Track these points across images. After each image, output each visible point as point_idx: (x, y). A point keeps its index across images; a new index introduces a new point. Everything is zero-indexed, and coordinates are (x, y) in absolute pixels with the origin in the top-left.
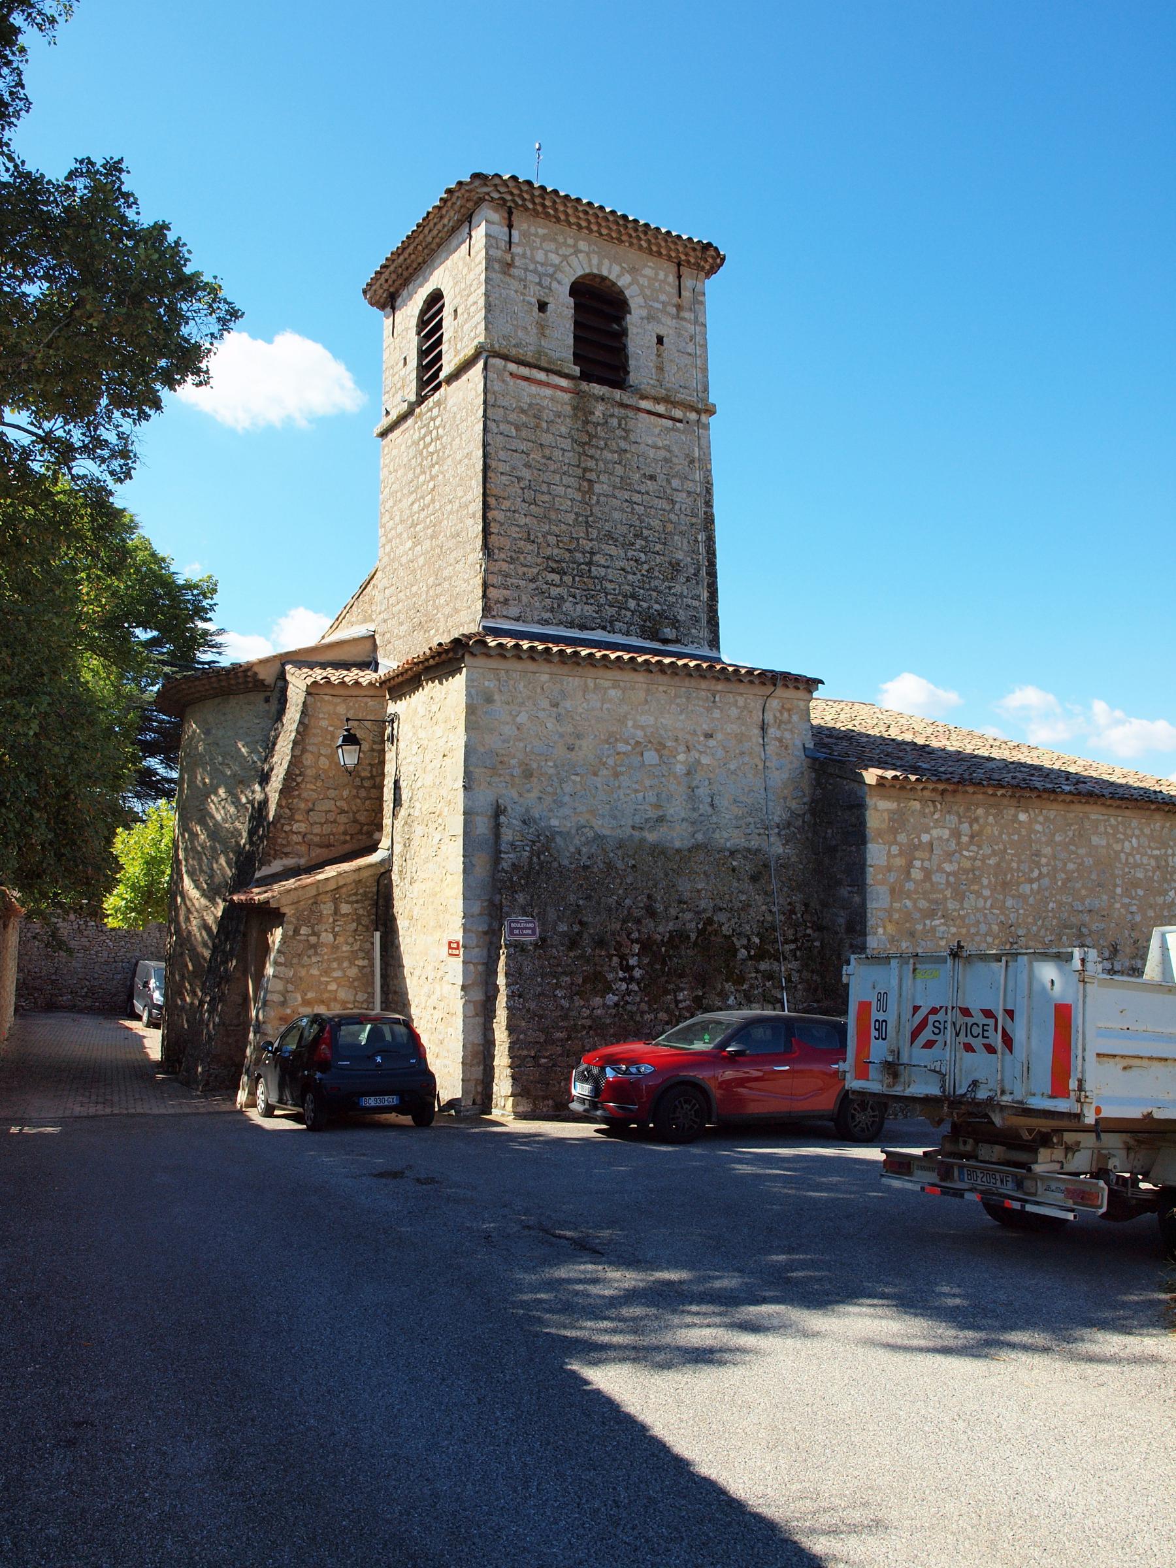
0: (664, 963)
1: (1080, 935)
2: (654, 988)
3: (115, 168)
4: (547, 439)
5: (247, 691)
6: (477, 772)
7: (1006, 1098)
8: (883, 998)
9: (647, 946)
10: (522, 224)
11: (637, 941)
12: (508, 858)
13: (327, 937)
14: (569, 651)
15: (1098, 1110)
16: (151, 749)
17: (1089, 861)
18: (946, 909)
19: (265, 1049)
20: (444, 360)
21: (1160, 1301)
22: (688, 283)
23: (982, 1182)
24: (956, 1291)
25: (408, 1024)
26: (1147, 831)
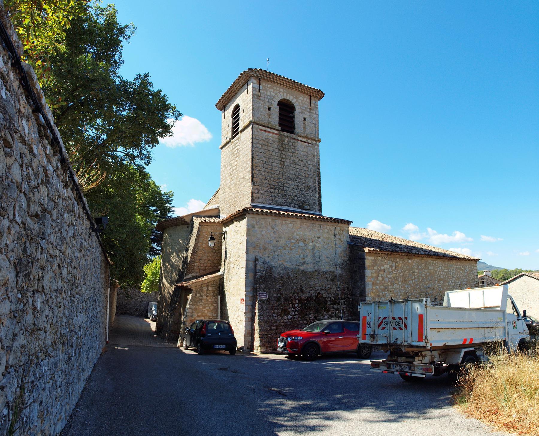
0: (305, 306)
1: (426, 295)
2: (303, 314)
3: (147, 76)
4: (271, 149)
5: (182, 224)
6: (250, 248)
7: (406, 343)
8: (370, 315)
9: (300, 301)
10: (263, 84)
11: (297, 299)
12: (259, 274)
13: (204, 297)
14: (277, 212)
15: (431, 344)
16: (154, 241)
17: (428, 274)
18: (388, 288)
19: (186, 329)
20: (240, 125)
21: (449, 398)
22: (313, 102)
23: (399, 368)
24: (393, 402)
25: (228, 324)
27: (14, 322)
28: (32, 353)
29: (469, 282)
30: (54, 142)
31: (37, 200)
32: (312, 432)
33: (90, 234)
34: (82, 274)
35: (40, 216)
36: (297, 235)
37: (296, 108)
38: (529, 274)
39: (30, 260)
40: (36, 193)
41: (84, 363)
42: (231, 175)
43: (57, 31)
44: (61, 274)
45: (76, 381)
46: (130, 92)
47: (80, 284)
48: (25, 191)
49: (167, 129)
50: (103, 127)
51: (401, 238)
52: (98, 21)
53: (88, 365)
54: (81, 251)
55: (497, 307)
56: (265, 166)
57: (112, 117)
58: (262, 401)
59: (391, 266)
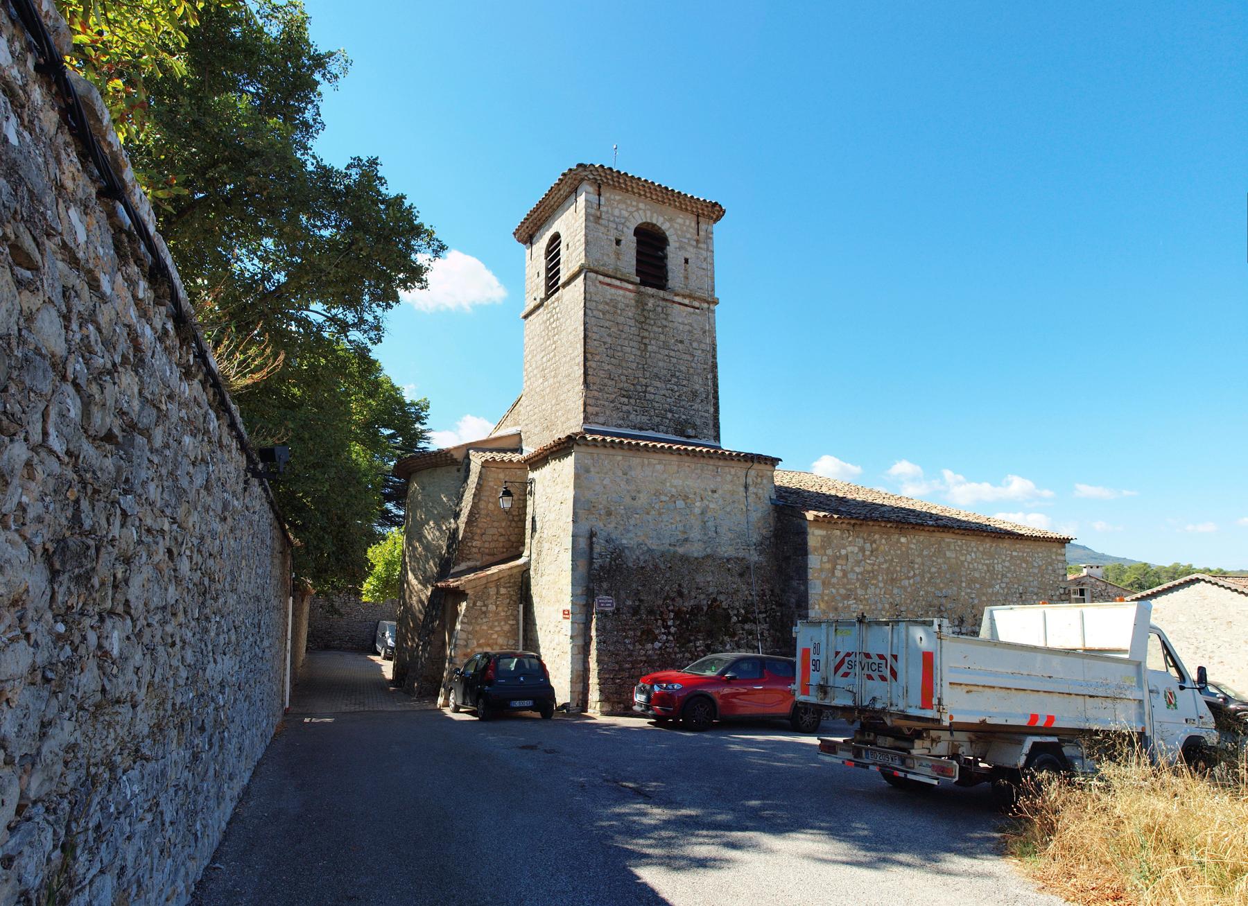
0: (688, 624)
1: (940, 611)
2: (683, 639)
3: (373, 162)
4: (621, 319)
5: (447, 465)
6: (581, 512)
8: (817, 647)
9: (678, 614)
10: (606, 194)
12: (598, 562)
13: (492, 608)
15: (951, 717)
16: (388, 498)
17: (944, 567)
20: (561, 274)
22: (703, 226)
23: (880, 759)
25: (539, 658)
27: (45, 694)
28: (98, 760)
29: (1045, 590)
30: (157, 274)
31: (110, 402)
32: (701, 871)
33: (246, 482)
34: (227, 570)
35: (120, 439)
36: (672, 486)
38: (1218, 578)
39: (91, 543)
40: (109, 387)
41: (232, 761)
42: (543, 370)
43: (166, 26)
44: (175, 570)
45: (212, 803)
46: (338, 192)
47: (223, 590)
48: (75, 378)
49: (415, 275)
50: (278, 257)
51: (883, 490)
52: (266, 30)
53: (242, 765)
54: (225, 519)
55: (1119, 651)
56: (610, 352)
57: (298, 239)
58: (604, 806)
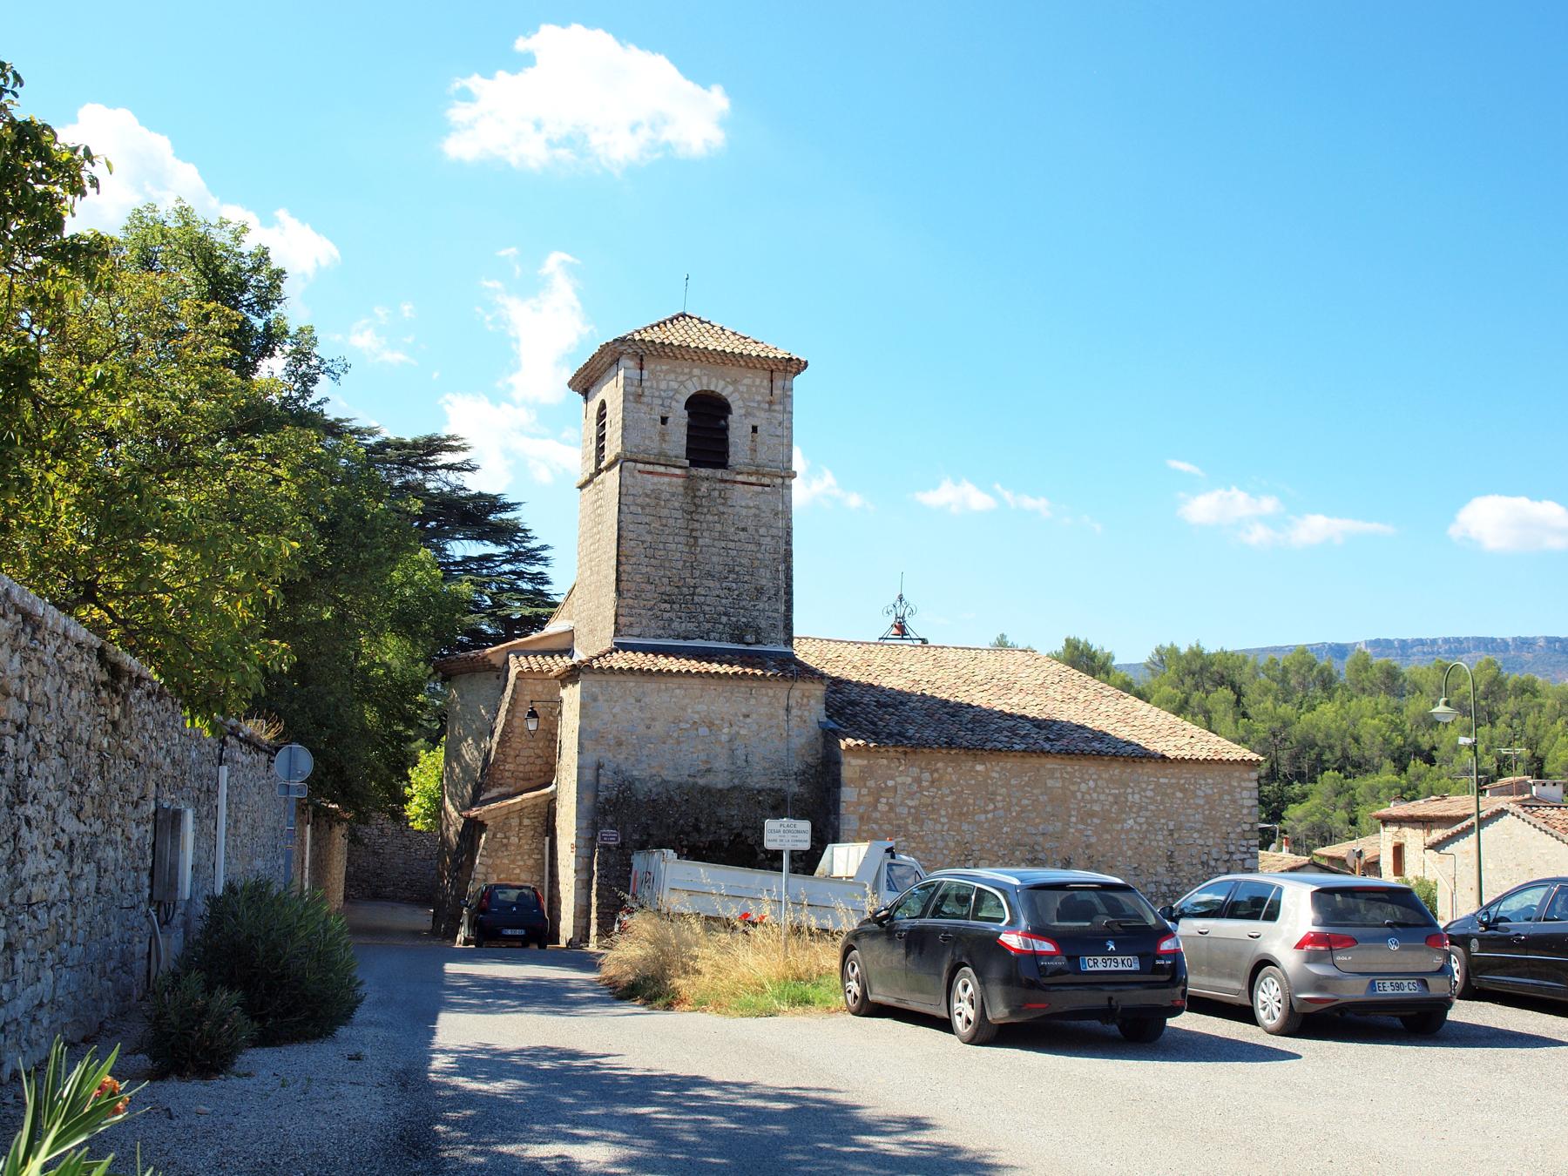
4: (664, 512)
6: (586, 743)
10: (650, 365)
13: (514, 840)
22: (778, 383)
26: (1106, 776)
37: (733, 407)
56: (650, 552)
59: (918, 780)
